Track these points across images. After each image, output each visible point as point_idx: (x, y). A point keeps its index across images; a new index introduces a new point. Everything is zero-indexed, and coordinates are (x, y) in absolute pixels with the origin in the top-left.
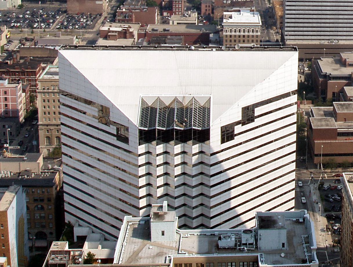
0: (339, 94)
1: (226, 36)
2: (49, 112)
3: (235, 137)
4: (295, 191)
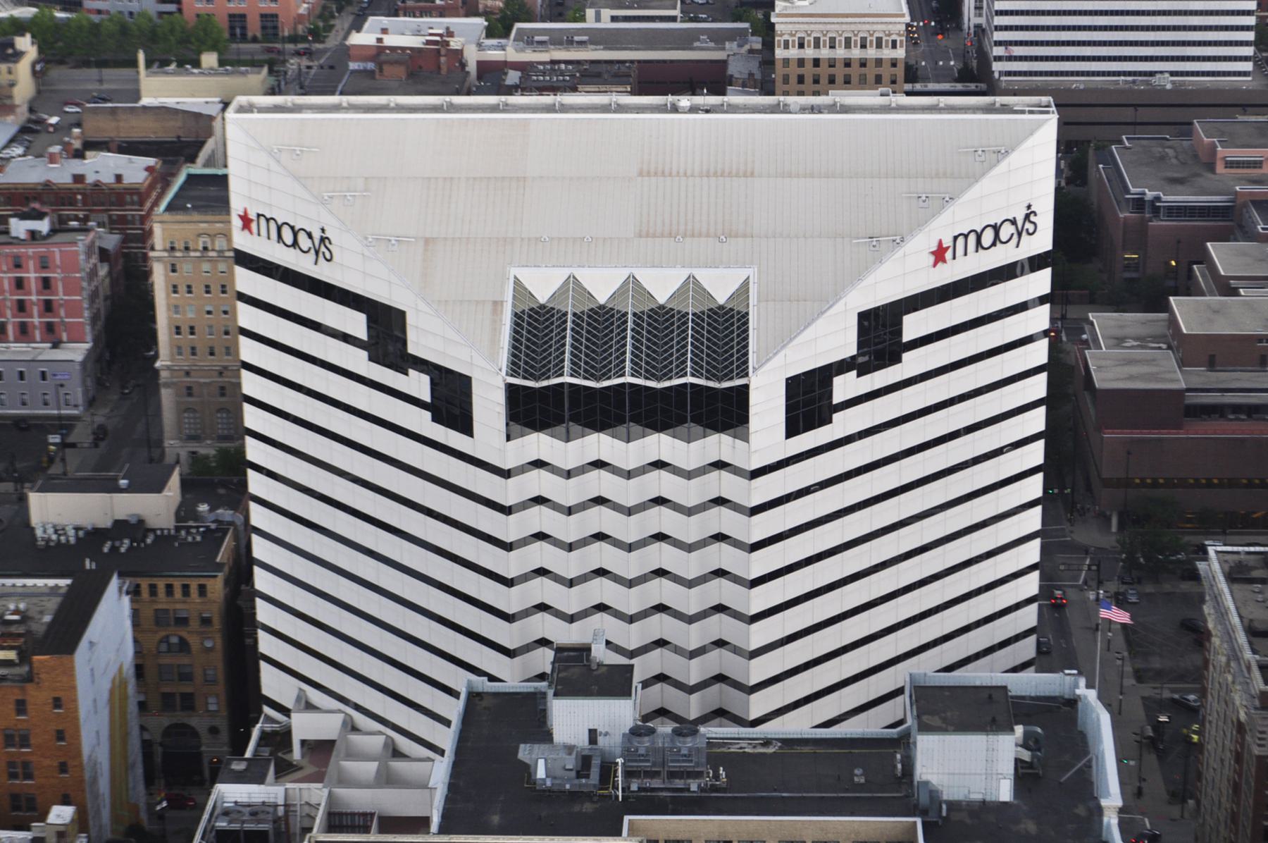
0: (1191, 271)
1: (786, 61)
2: (192, 328)
3: (836, 416)
4: (1039, 605)
